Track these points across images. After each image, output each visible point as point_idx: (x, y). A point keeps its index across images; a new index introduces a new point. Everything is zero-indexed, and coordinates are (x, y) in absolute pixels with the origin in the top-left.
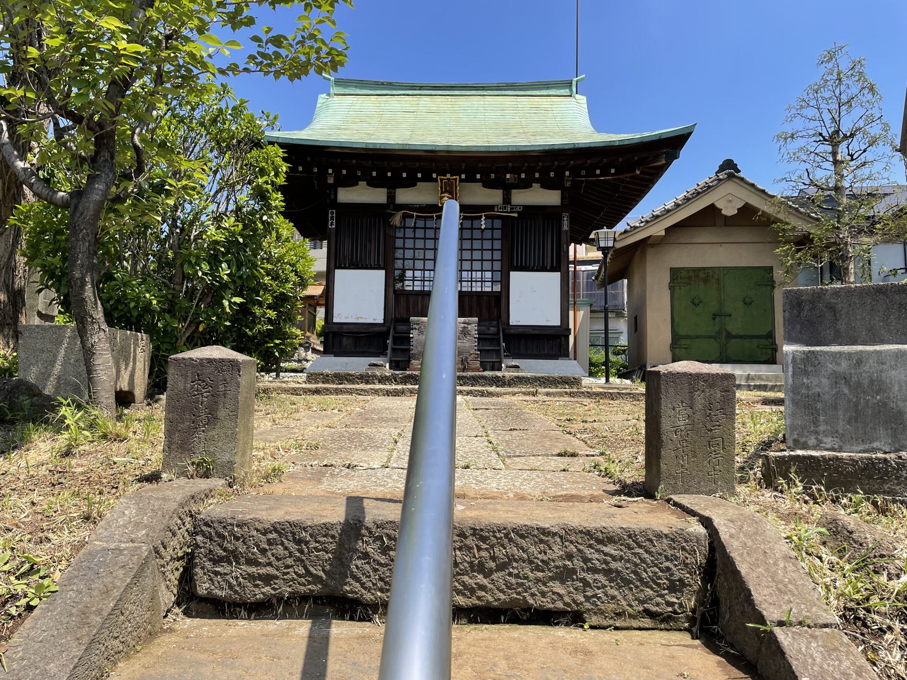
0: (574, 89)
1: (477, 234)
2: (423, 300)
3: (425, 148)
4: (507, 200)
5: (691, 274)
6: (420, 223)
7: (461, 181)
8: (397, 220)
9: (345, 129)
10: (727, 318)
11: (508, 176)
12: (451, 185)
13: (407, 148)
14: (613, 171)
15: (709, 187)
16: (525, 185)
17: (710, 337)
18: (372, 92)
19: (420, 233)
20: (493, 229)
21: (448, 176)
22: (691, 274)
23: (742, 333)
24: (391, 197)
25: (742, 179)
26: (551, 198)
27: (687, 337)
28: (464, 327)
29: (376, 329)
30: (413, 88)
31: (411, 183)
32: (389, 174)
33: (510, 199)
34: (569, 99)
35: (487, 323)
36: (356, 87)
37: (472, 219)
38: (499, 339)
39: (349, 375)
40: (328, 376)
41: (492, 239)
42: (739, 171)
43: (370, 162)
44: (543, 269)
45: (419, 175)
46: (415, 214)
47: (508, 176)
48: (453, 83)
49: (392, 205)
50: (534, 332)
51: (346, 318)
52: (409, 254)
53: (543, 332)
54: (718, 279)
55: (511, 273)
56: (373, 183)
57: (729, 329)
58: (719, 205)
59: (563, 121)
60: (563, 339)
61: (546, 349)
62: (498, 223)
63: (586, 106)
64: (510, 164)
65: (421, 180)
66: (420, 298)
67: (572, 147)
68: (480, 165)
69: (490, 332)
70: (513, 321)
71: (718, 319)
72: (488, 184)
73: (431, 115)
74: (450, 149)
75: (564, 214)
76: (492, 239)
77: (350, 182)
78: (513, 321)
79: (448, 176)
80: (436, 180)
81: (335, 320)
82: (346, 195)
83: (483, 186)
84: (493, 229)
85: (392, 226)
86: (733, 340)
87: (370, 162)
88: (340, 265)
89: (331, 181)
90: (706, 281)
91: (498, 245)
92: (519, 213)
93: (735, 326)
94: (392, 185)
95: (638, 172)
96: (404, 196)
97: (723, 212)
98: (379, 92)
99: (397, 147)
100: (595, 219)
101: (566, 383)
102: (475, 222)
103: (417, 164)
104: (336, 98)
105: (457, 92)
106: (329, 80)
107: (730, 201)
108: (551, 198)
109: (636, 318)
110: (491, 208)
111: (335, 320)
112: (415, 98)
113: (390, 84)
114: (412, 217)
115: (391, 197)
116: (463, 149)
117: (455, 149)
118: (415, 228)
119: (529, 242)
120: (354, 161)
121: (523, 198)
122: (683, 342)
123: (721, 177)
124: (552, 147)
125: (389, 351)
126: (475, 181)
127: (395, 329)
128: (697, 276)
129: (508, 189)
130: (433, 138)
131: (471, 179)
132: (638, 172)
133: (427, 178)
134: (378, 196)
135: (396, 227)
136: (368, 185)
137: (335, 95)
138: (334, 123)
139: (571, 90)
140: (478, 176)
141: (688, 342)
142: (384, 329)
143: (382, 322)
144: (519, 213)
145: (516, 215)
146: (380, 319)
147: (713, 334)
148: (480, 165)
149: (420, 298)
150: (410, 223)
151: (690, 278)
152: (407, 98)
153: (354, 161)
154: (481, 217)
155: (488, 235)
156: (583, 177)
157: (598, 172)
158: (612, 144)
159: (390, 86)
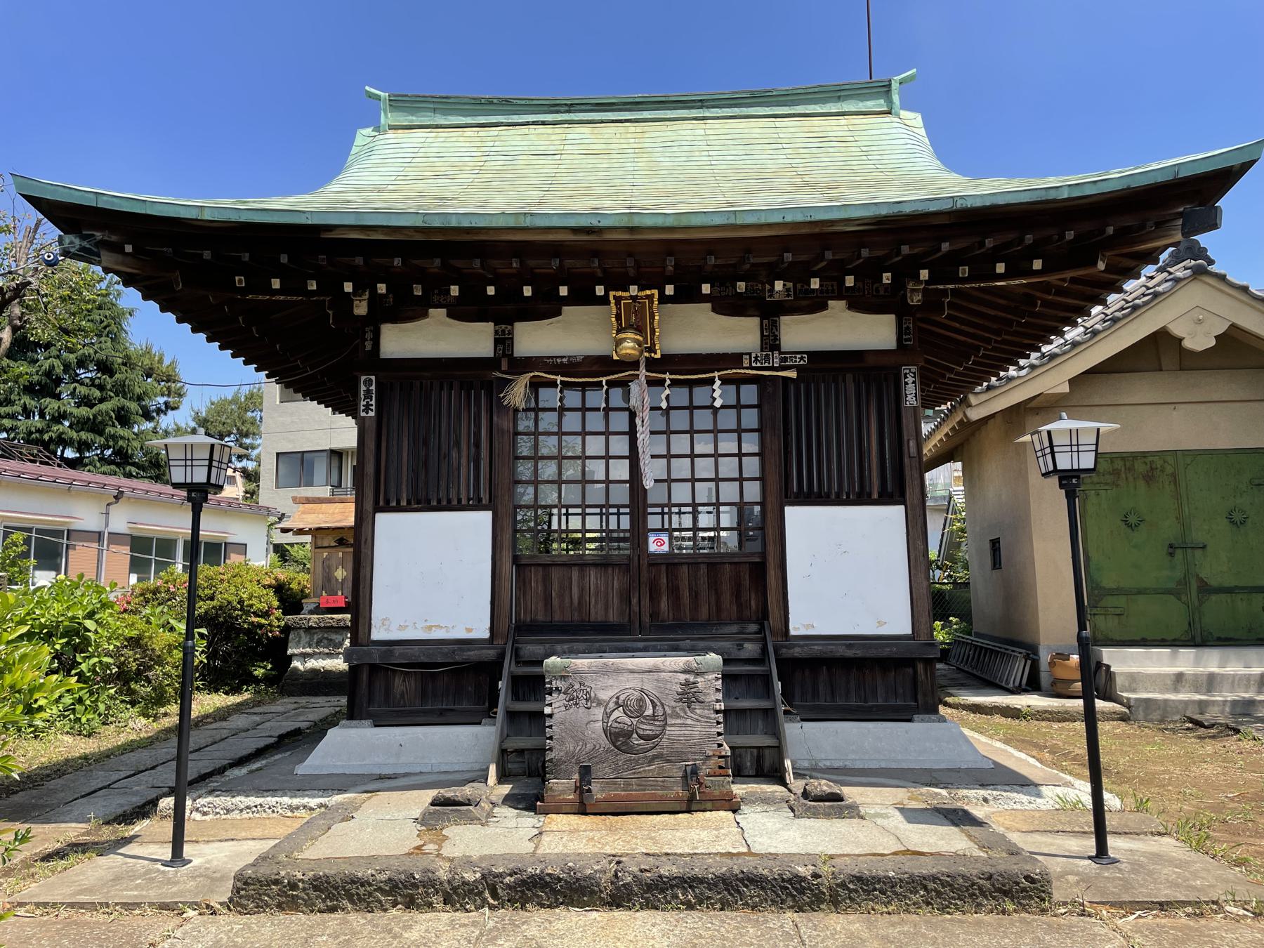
0: (896, 98)
1: (703, 420)
2: (582, 577)
3: (572, 223)
4: (770, 341)
5: (1119, 464)
6: (573, 398)
7: (664, 299)
8: (517, 393)
9: (394, 191)
10: (1198, 553)
11: (779, 285)
12: (640, 313)
13: (528, 222)
14: (1037, 265)
15: (1156, 295)
16: (814, 305)
17: (1168, 592)
18: (469, 120)
19: (572, 421)
20: (738, 406)
21: (634, 290)
22: (1119, 464)
23: (1229, 582)
24: (503, 341)
25: (1222, 278)
26: (876, 332)
27: (1117, 592)
28: (687, 683)
29: (472, 655)
30: (554, 108)
31: (546, 308)
32: (491, 290)
33: (776, 338)
34: (887, 119)
35: (735, 628)
36: (435, 110)
37: (691, 384)
38: (767, 679)
39: (354, 881)
40: (293, 886)
41: (739, 431)
42: (1211, 262)
43: (438, 262)
44: (861, 498)
45: (564, 291)
46: (559, 379)
47: (779, 285)
48: (638, 96)
49: (506, 361)
50: (849, 653)
51: (402, 628)
52: (548, 470)
53: (872, 653)
54: (1174, 475)
55: (789, 510)
56: (463, 311)
57: (1202, 575)
58: (1176, 330)
59: (876, 159)
60: (920, 667)
61: (880, 691)
62: (750, 393)
63: (923, 132)
64: (788, 257)
65: (569, 301)
66: (575, 574)
67: (947, 206)
68: (712, 260)
69: (744, 655)
70: (799, 624)
71: (1179, 553)
72: (727, 306)
73: (591, 159)
74: (636, 222)
75: (905, 369)
76: (739, 431)
77: (406, 309)
78: (799, 624)
79: (634, 290)
80: (604, 301)
81: (376, 635)
82: (400, 342)
83: (714, 310)
84: (738, 406)
85: (507, 408)
86: (1214, 598)
87: (438, 262)
88: (387, 502)
89: (361, 309)
90: (1149, 478)
91: (751, 444)
92: (799, 369)
93: (1215, 569)
94: (506, 313)
95: (1101, 266)
96: (534, 339)
97: (1187, 344)
98: (482, 120)
99: (501, 223)
100: (951, 370)
101: (1006, 893)
102: (698, 391)
103: (555, 263)
104: (391, 135)
105: (646, 115)
106: (378, 98)
107: (1200, 322)
108: (876, 332)
109: (995, 544)
110: (734, 359)
111: (376, 635)
112: (558, 129)
113: (507, 102)
114: (553, 384)
115: (503, 341)
116: (669, 222)
117: (649, 222)
118: (562, 410)
119: (834, 438)
120: (397, 262)
121: (805, 334)
122: (1110, 601)
123: (1179, 274)
124: (895, 210)
125: (500, 710)
126: (698, 298)
127: (516, 652)
128: (1130, 469)
129: (770, 313)
130: (596, 203)
131: (688, 294)
132: (1101, 266)
133: (582, 297)
134: (474, 340)
135: (516, 410)
136: (449, 315)
137: (392, 128)
138: (376, 180)
139: (890, 101)
140: (706, 289)
141: (1121, 601)
142: (490, 654)
143: (487, 635)
144: (799, 369)
145: (792, 374)
146: (480, 629)
147: (1172, 585)
148: (712, 260)
149: (575, 574)
150: (549, 397)
151: (1116, 473)
152: (541, 129)
153: (397, 262)
154: (711, 382)
155: (728, 419)
156: (964, 280)
157: (1000, 268)
158: (1052, 195)
159: (507, 105)
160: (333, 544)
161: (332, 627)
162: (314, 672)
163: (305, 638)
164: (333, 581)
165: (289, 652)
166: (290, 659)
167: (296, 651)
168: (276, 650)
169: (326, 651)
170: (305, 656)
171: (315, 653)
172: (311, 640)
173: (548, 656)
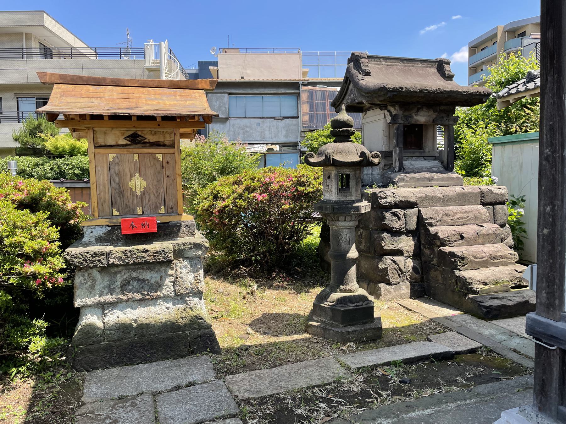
160: (122, 142)
161: (146, 262)
162: (124, 328)
163: (101, 281)
164: (128, 195)
165: (78, 303)
166: (76, 313)
167: (89, 301)
168: (58, 308)
169: (138, 296)
170: (103, 307)
171: (120, 301)
172: (112, 282)
173: (380, 282)
